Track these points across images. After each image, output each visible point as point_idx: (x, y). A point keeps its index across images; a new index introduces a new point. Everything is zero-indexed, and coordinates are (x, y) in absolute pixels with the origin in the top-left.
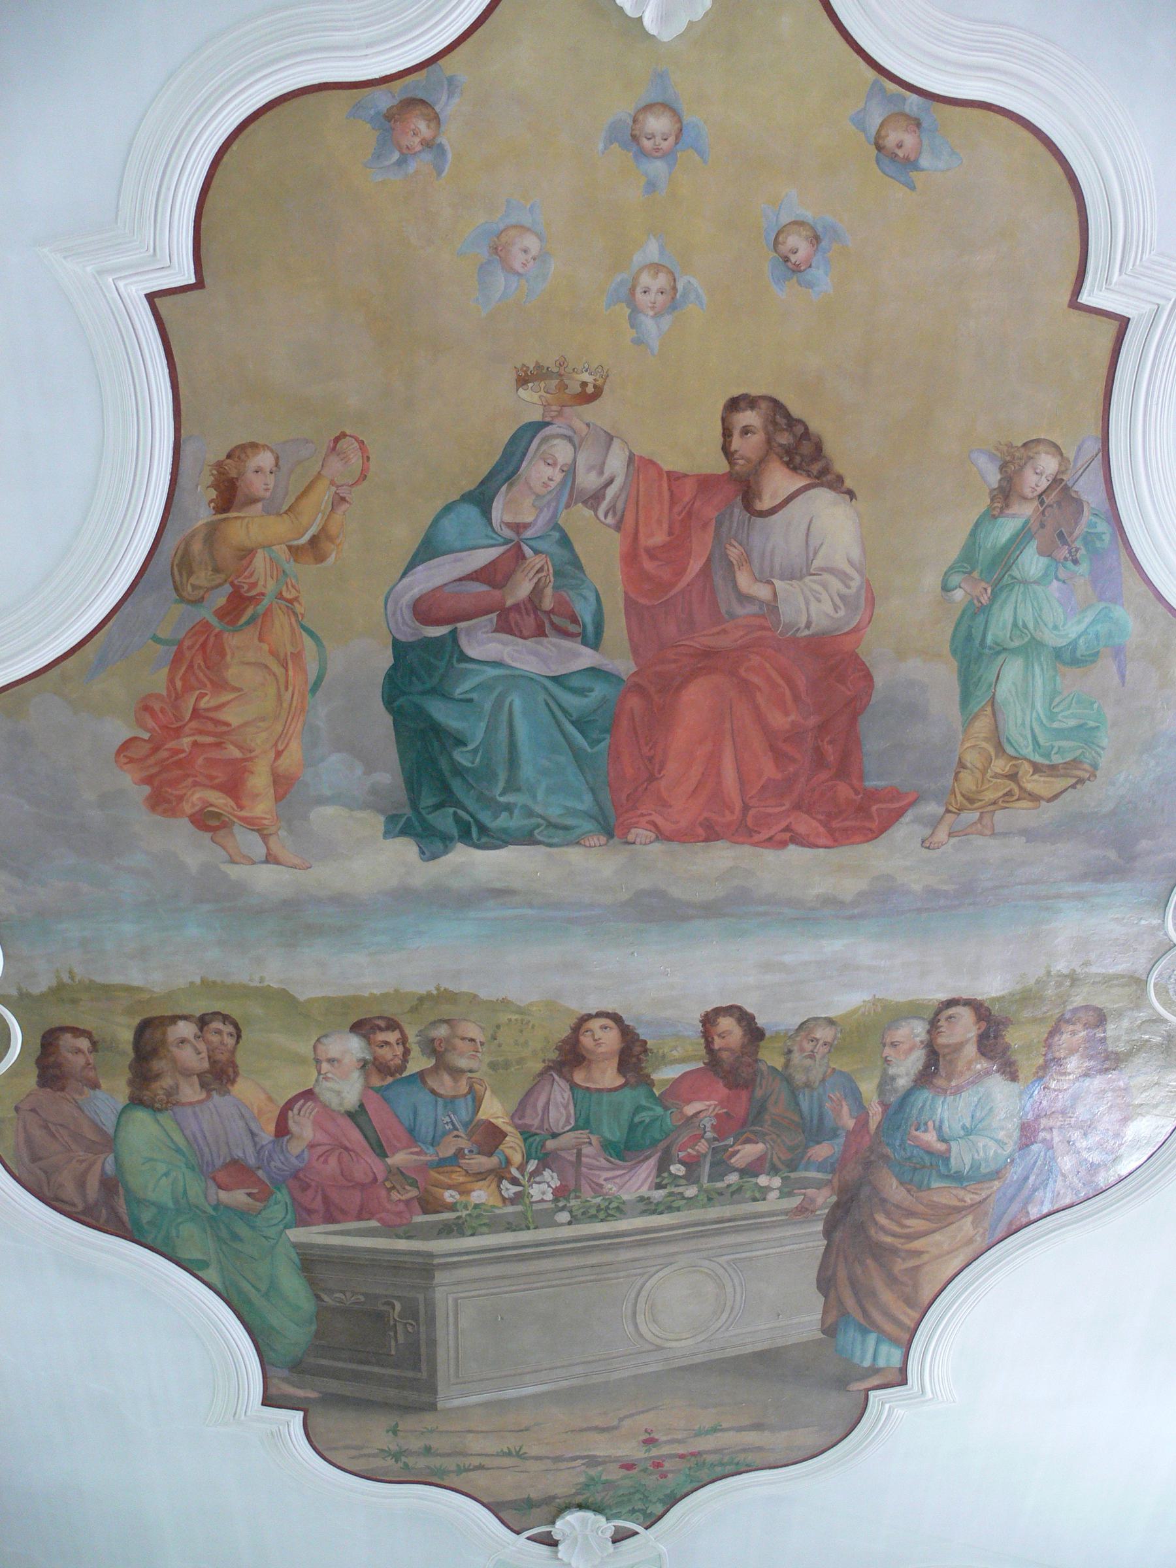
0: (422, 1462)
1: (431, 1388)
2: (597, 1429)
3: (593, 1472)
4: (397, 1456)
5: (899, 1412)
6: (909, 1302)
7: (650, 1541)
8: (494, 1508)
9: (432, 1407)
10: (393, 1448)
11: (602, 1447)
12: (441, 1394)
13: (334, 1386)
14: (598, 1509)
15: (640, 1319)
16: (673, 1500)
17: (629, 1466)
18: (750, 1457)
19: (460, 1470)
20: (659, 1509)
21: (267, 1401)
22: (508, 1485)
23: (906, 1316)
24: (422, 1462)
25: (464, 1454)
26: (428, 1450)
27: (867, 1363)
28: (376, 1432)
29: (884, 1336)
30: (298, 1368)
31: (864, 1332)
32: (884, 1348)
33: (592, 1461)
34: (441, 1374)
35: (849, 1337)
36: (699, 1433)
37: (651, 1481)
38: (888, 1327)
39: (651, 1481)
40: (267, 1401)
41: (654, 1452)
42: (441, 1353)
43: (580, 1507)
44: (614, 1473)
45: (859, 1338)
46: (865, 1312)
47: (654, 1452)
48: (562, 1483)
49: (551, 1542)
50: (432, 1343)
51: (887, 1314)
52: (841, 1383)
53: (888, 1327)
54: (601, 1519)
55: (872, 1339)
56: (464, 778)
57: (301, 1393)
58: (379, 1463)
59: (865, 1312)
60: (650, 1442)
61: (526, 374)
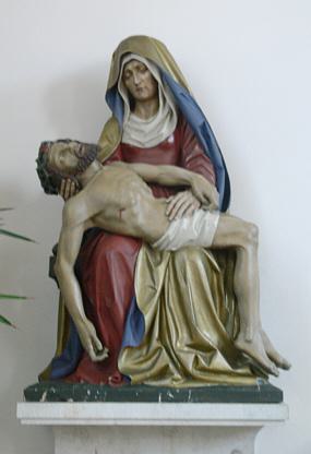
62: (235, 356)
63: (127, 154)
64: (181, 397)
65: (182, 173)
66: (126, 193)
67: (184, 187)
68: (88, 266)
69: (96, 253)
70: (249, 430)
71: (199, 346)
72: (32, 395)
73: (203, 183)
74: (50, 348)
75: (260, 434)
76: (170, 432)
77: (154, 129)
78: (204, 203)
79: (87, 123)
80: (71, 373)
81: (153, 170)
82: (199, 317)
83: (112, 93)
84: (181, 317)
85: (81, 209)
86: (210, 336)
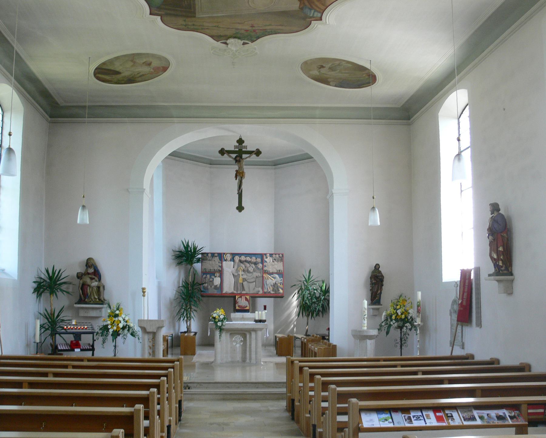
0: (192, 27)
1: (194, 13)
2: (239, 23)
3: (237, 31)
4: (185, 25)
5: (319, 26)
6: (323, 5)
7: (251, 45)
8: (212, 37)
9: (195, 17)
10: (184, 24)
11: (240, 27)
12: (197, 14)
13: (169, 12)
14: (239, 38)
15: (250, 3)
16: (258, 38)
17: (247, 31)
18: (279, 31)
19: (202, 29)
20: (255, 39)
21: (151, 14)
22: (215, 32)
23: (323, 7)
24: (192, 27)
25: (203, 26)
26: (194, 25)
27: (311, 15)
28: (181, 21)
29: (316, 11)
30: (159, 8)
31: (310, 9)
32: (316, 13)
33: (237, 29)
34: (197, 11)
35: (307, 11)
36: (266, 26)
37: (253, 34)
38: (317, 9)
39: (253, 34)
40: (151, 14)
41: (254, 28)
42: (197, 7)
43: (235, 37)
44: (243, 32)
45: (309, 11)
46: (311, 6)
47: (254, 28)
48: (228, 33)
49: (226, 43)
50: (194, 4)
51: (317, 6)
52: (304, 19)
53: (317, 9)
54: (240, 41)
55: (313, 11)
56: (462, 151)
57: (160, 13)
58: (180, 27)
59: (311, 6)
60: (252, 26)
61: (406, 317)
62: (100, 300)
63: (88, 274)
64: (92, 304)
65: (94, 277)
66: (87, 280)
67: (94, 279)
68: (82, 289)
69: (84, 287)
70: (101, 308)
71: (95, 298)
72: (76, 304)
73: (96, 278)
74: (78, 298)
75: (385, 334)
76: (93, 308)
77: (91, 270)
78: (96, 281)
79: (82, 270)
80: (80, 301)
81: (90, 276)
82: (252, 419)
83: (86, 265)
84: (228, 387)
85: (81, 282)
86: (96, 297)
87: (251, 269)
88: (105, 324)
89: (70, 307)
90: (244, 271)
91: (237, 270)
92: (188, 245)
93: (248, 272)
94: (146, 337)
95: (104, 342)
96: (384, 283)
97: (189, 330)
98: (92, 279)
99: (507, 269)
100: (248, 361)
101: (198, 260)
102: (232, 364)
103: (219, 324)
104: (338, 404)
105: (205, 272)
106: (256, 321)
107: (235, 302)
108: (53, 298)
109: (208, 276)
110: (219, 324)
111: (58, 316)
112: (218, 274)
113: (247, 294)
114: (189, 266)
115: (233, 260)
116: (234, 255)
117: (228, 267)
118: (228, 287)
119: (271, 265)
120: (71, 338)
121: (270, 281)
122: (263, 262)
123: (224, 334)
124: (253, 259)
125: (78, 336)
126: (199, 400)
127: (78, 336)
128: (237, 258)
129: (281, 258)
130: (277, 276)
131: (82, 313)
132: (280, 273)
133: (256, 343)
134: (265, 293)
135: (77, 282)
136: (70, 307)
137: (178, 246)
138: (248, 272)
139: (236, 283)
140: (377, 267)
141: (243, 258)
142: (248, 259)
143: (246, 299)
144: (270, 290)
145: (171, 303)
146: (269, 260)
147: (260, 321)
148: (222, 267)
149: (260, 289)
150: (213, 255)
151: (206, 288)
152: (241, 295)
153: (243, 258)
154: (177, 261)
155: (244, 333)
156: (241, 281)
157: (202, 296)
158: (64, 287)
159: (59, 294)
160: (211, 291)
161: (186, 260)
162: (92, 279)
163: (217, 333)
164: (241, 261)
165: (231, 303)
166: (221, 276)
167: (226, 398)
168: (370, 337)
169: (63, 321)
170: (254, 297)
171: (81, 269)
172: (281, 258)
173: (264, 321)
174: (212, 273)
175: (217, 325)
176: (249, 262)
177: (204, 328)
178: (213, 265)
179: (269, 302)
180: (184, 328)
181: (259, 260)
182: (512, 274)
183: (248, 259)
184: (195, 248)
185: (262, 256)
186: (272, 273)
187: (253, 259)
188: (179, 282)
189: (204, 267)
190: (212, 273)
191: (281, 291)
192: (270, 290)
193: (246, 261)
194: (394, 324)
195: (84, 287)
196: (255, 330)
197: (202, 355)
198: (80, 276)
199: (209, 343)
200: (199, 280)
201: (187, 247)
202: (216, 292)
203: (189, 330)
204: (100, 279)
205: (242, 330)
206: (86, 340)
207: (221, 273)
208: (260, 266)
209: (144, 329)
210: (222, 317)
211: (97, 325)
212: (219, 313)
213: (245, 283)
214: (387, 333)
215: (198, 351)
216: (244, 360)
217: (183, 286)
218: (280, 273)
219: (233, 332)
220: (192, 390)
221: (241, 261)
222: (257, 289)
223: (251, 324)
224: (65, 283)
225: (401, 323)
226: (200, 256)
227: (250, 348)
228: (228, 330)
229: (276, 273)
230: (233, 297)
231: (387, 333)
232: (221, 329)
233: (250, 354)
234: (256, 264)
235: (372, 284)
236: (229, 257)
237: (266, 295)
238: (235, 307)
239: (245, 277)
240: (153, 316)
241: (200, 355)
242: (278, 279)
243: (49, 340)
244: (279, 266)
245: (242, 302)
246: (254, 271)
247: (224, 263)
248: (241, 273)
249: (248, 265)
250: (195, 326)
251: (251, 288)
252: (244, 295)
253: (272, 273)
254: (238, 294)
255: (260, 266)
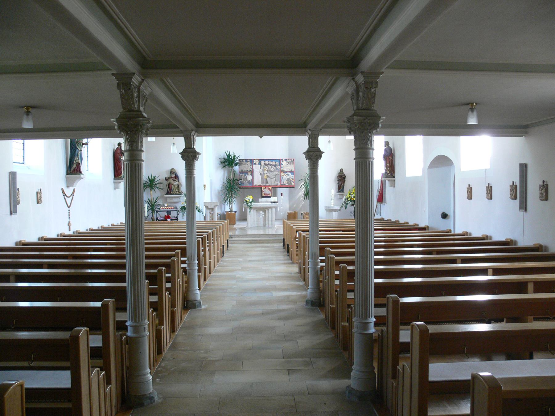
63: (172, 178)
66: (171, 181)
69: (169, 185)
77: (173, 176)
80: (168, 193)
87: (272, 170)
88: (183, 205)
89: (162, 197)
90: (267, 171)
91: (263, 171)
92: (229, 155)
93: (271, 171)
94: (208, 211)
95: (183, 215)
96: (346, 180)
97: (231, 210)
98: (174, 180)
99: (391, 174)
100: (267, 226)
101: (237, 165)
102: (258, 227)
103: (249, 204)
104: (375, 278)
105: (241, 172)
106: (272, 202)
107: (262, 191)
108: (152, 192)
109: (244, 175)
110: (249, 204)
111: (155, 202)
112: (250, 173)
113: (269, 186)
114: (230, 168)
115: (260, 164)
116: (260, 160)
117: (257, 168)
118: (257, 182)
119: (286, 166)
120: (166, 213)
121: (285, 177)
122: (280, 164)
123: (252, 210)
124: (274, 163)
125: (169, 212)
126: (237, 243)
127: (169, 212)
128: (263, 162)
129: (293, 162)
130: (290, 174)
131: (169, 200)
132: (292, 172)
133: (271, 214)
134: (282, 185)
135: (166, 183)
136: (162, 197)
137: (223, 155)
138: (271, 171)
139: (262, 179)
140: (341, 170)
141: (267, 162)
142: (270, 163)
143: (269, 189)
144: (286, 183)
145: (219, 193)
146: (284, 163)
147: (274, 202)
148: (252, 168)
149: (279, 183)
150: (246, 160)
151: (242, 183)
152: (266, 187)
153: (267, 162)
154: (223, 165)
155: (265, 210)
156: (265, 178)
157: (240, 188)
158: (158, 186)
159: (156, 190)
160: (246, 184)
161: (228, 165)
162: (174, 180)
163: (248, 210)
164: (265, 164)
165: (259, 192)
166: (252, 175)
167: (252, 242)
168: (335, 210)
169: (158, 205)
170: (275, 188)
171: (168, 175)
172: (293, 162)
173: (277, 202)
174: (246, 173)
175: (248, 205)
176: (271, 165)
177: (241, 208)
178: (247, 167)
179: (285, 191)
180: (227, 209)
181: (277, 163)
182: (394, 177)
183: (270, 163)
184: (234, 157)
185: (280, 160)
186: (287, 172)
187: (274, 163)
188: (224, 179)
189: (241, 169)
190: (246, 173)
191: (293, 184)
192: (286, 183)
193: (269, 164)
194: (350, 203)
195: (169, 185)
196: (271, 208)
197: (239, 225)
198: (167, 179)
199: (244, 218)
200: (237, 177)
201: (229, 156)
202: (248, 185)
203: (231, 210)
204: (179, 181)
205: (263, 208)
206: (173, 214)
207: (252, 172)
208: (278, 167)
209: (207, 207)
210: (251, 200)
211: (179, 206)
212: (249, 198)
213: (268, 179)
214: (346, 208)
215: (237, 223)
216: (265, 225)
217: (227, 182)
218: (292, 172)
219: (258, 209)
220: (233, 239)
221: (265, 164)
222: (276, 183)
223: (270, 205)
224: (158, 183)
225: (353, 203)
226: (238, 161)
227: (268, 218)
228: (254, 208)
229: (290, 172)
230: (260, 188)
231: (346, 208)
232: (250, 207)
233: (268, 222)
234: (275, 166)
235: (338, 180)
236: (257, 162)
237: (282, 187)
238: (262, 194)
239: (268, 174)
240: (208, 200)
241: (238, 224)
242: (291, 176)
243: (151, 216)
244: (291, 167)
245: (266, 191)
246: (274, 170)
247: (254, 166)
248: (265, 172)
249: (270, 167)
250: (235, 207)
251: (272, 182)
252: (268, 186)
253: (287, 172)
254: (264, 186)
255: (278, 167)
